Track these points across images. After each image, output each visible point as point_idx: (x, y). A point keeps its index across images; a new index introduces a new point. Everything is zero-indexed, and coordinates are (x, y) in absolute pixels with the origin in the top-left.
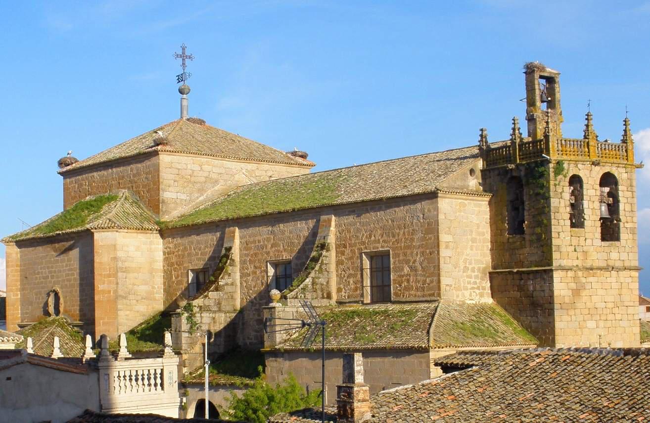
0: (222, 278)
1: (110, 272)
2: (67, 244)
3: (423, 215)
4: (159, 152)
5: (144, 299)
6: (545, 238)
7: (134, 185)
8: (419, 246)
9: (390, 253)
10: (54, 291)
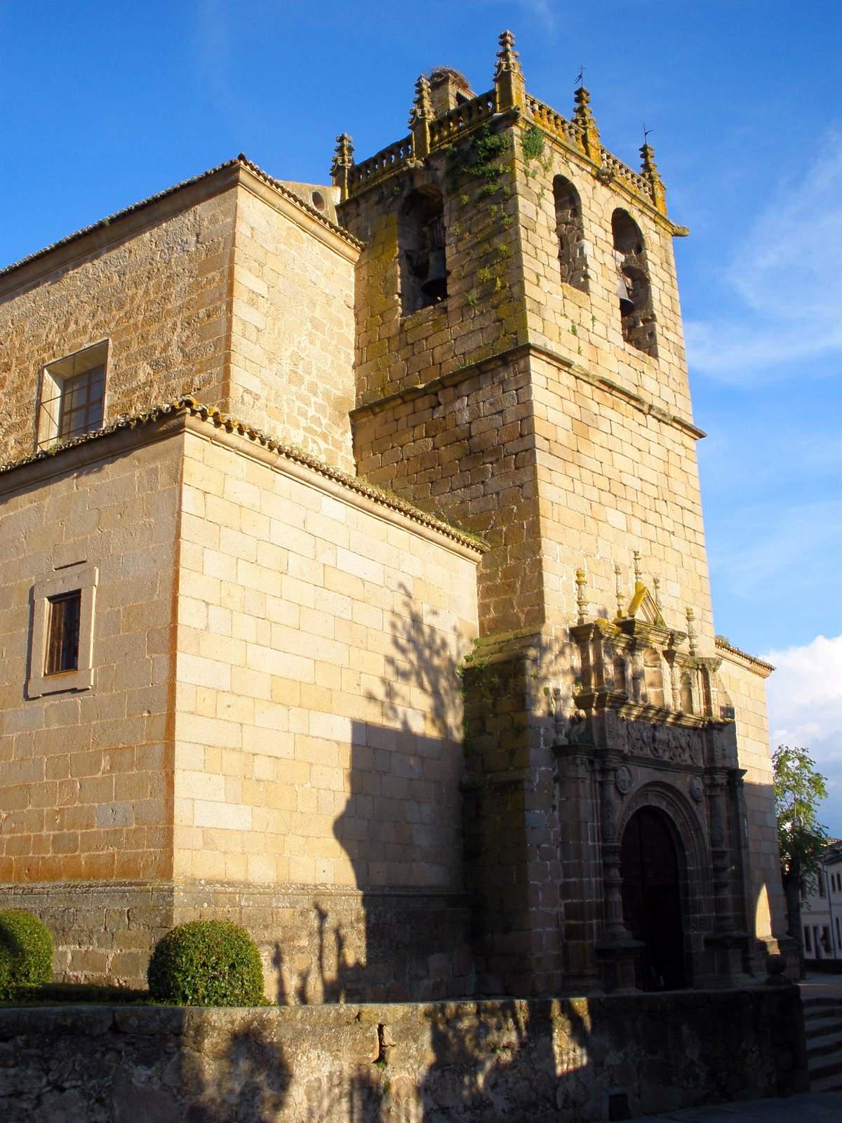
3: (198, 236)
6: (503, 287)
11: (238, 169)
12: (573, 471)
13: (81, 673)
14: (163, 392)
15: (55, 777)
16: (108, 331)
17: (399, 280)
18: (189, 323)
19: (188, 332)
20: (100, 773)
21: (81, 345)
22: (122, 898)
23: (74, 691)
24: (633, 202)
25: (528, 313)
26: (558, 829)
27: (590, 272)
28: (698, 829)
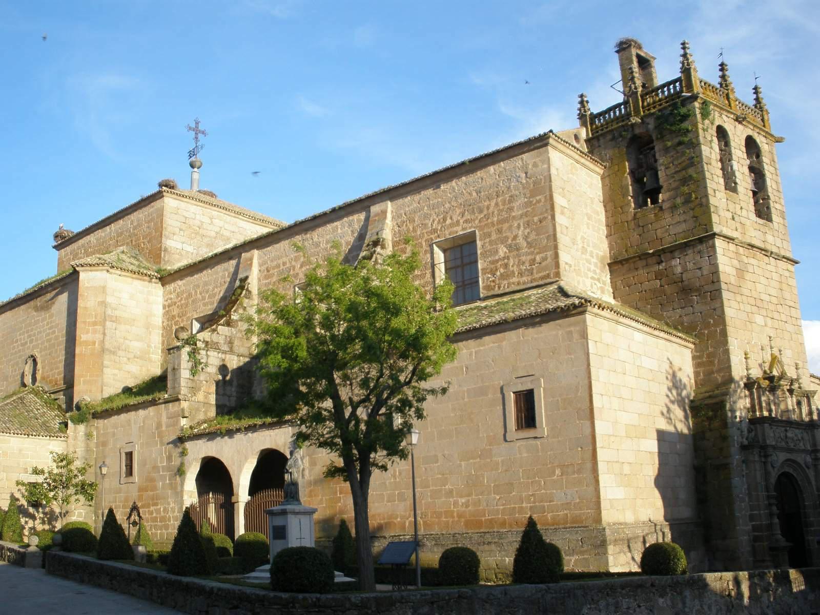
0: (235, 311)
1: (96, 318)
2: (49, 296)
3: (526, 173)
4: (164, 194)
5: (137, 358)
6: (696, 198)
7: (134, 239)
8: (521, 216)
9: (475, 234)
10: (32, 356)
11: (549, 137)
12: (739, 298)
13: (538, 430)
14: (517, 263)
15: (528, 478)
16: (474, 225)
17: (630, 188)
18: (528, 225)
19: (528, 230)
20: (555, 477)
21: (457, 232)
22: (576, 533)
23: (536, 438)
24: (755, 129)
25: (712, 214)
26: (746, 487)
27: (737, 180)
28: (810, 483)
